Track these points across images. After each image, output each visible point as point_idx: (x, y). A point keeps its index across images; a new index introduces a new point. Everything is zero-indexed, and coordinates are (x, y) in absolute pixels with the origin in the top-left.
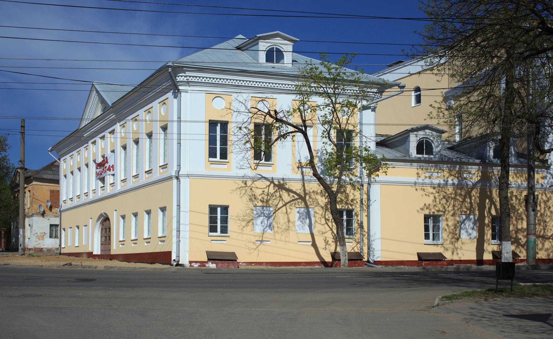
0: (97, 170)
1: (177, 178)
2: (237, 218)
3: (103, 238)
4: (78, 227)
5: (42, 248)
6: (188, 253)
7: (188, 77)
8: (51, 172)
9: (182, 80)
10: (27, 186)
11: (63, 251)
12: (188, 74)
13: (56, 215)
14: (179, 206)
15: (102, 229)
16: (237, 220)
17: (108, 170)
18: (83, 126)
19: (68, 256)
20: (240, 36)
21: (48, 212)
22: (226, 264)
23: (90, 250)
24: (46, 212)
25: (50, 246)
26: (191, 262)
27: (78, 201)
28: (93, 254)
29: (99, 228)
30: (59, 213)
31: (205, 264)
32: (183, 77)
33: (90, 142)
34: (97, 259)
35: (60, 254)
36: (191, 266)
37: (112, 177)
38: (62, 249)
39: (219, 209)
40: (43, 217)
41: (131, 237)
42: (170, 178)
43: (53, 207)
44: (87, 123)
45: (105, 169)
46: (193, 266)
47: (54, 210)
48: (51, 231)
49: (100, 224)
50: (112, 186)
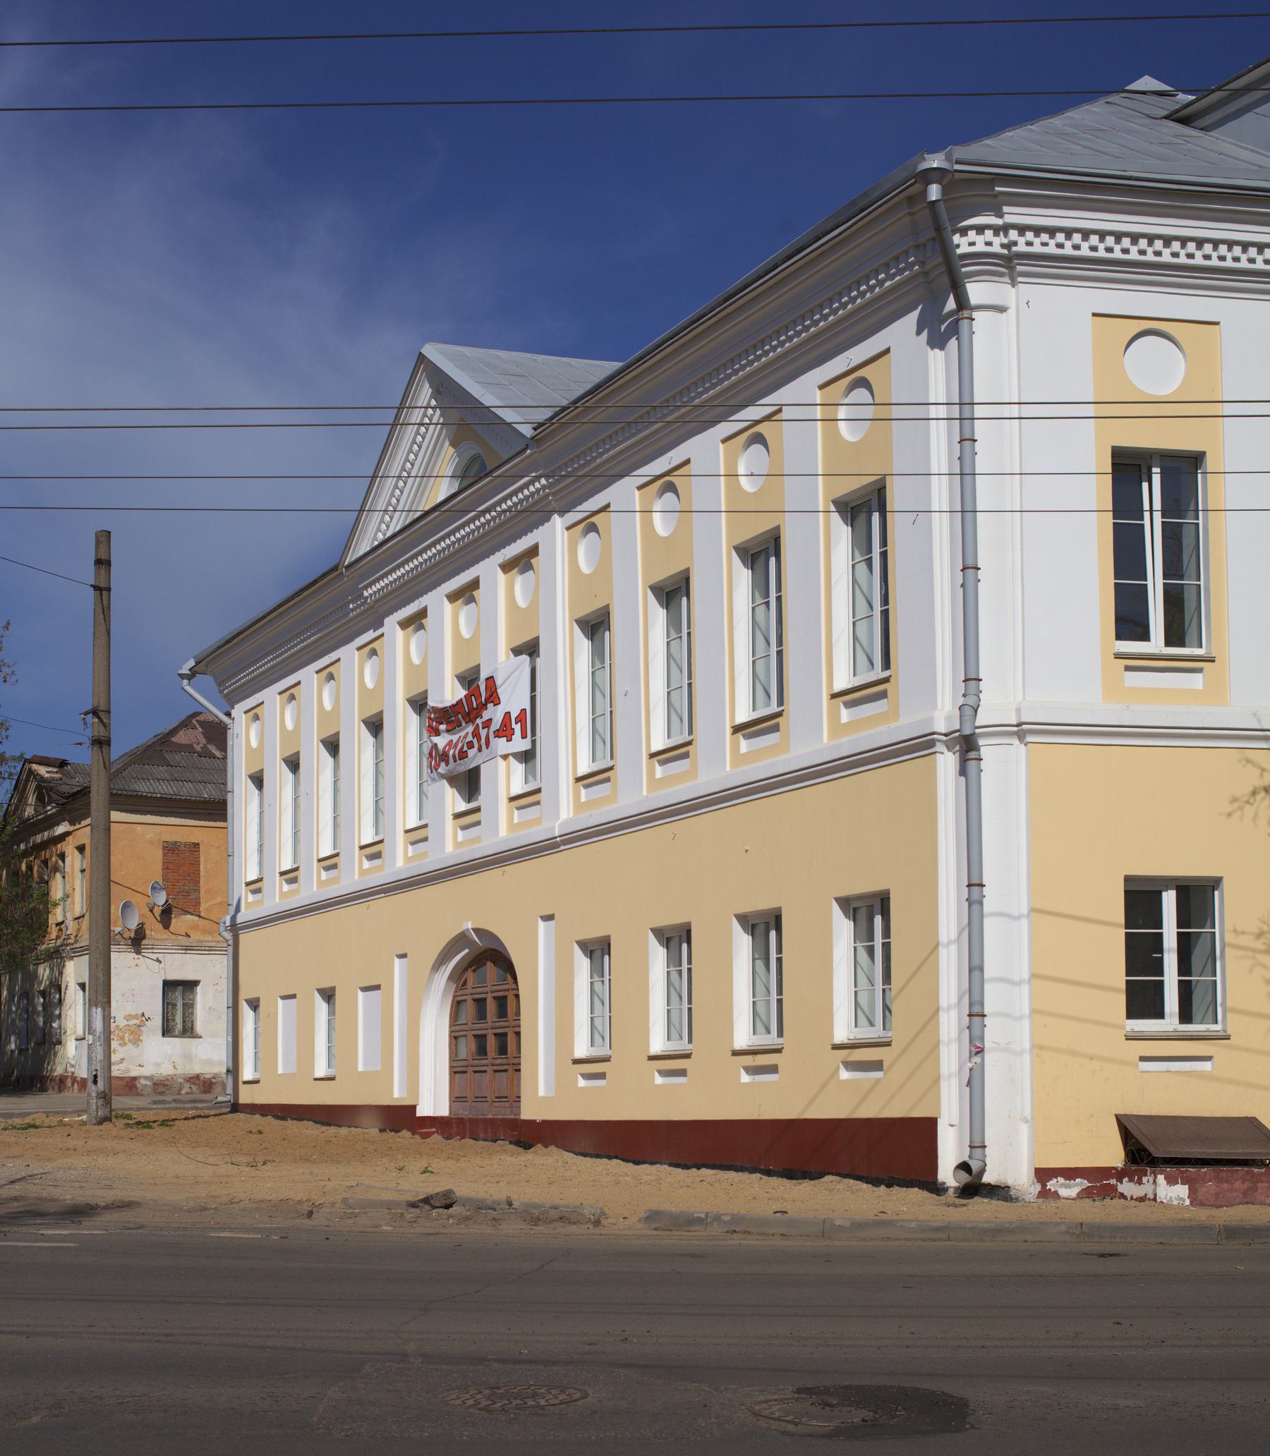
0: (436, 739)
1: (967, 745)
2: (1263, 940)
3: (462, 1041)
4: (328, 995)
5: (135, 1079)
6: (1024, 1130)
7: (1013, 234)
8: (162, 771)
9: (980, 247)
10: (72, 828)
11: (246, 1096)
12: (1014, 215)
13: (185, 941)
14: (975, 885)
15: (457, 1005)
16: (1260, 951)
17: (498, 734)
18: (361, 553)
19: (277, 1117)
20: (1147, 83)
21: (154, 930)
22: (1238, 1183)
23: (396, 1094)
24: (148, 932)
25: (166, 1070)
26: (1043, 1175)
27: (327, 882)
28: (419, 1114)
29: (444, 996)
30: (228, 936)
31: (1113, 1181)
32: (989, 233)
33: (391, 622)
34: (437, 1138)
35: (236, 1107)
36: (1045, 1194)
37: (518, 768)
38: (241, 1086)
39: (1169, 900)
40: (138, 952)
41: (645, 1040)
42: (922, 745)
43: (175, 911)
44: (380, 537)
45: (483, 733)
46: (1056, 1195)
47: (181, 922)
48: (168, 1006)
49: (450, 978)
50: (519, 808)
